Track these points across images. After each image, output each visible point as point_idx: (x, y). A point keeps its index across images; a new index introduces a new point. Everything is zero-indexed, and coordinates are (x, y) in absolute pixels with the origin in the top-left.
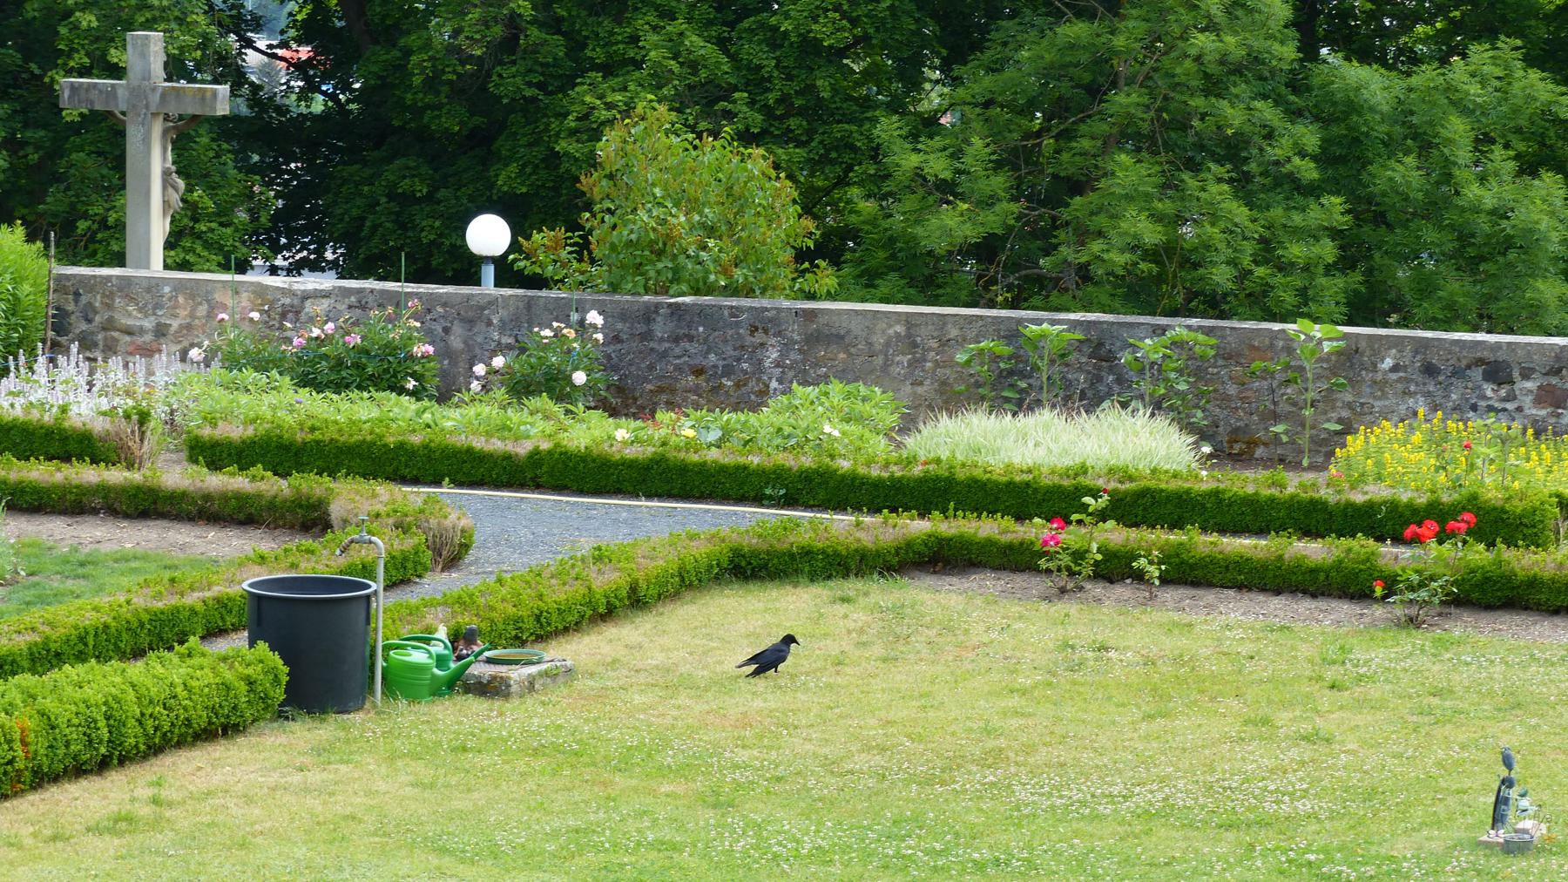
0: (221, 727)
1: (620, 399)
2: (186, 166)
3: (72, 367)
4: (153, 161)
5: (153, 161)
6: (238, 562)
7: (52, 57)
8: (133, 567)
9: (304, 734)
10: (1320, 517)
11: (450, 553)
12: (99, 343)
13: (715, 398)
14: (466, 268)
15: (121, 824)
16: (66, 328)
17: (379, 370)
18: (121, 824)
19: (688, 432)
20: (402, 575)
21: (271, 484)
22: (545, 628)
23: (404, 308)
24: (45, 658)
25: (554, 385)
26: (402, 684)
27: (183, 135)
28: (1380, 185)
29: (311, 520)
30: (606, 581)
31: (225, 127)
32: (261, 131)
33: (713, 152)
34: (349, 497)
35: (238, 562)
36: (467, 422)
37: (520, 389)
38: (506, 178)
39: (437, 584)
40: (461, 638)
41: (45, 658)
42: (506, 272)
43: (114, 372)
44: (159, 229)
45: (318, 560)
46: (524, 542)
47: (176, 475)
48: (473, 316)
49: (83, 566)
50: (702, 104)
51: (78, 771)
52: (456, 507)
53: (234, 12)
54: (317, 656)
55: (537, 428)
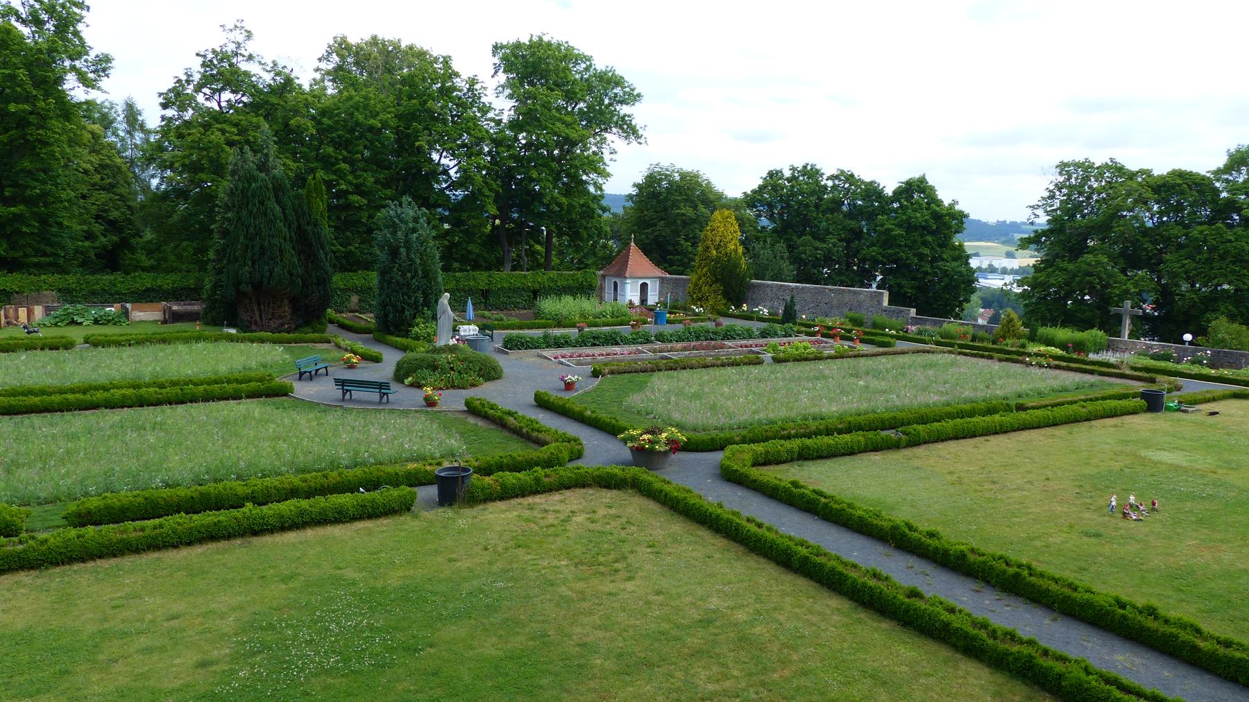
0: (1134, 412)
1: (1212, 366)
2: (1132, 322)
3: (1110, 353)
4: (1127, 322)
5: (1127, 322)
6: (1140, 387)
7: (1109, 304)
8: (1119, 385)
9: (1149, 415)
10: (1193, 196)
11: (1178, 389)
12: (1115, 350)
13: (1231, 366)
14: (1183, 342)
15: (1116, 426)
16: (1110, 347)
17: (1167, 358)
18: (1116, 426)
19: (1226, 372)
20: (1169, 391)
21: (1148, 374)
22: (1196, 402)
23: (1172, 348)
24: (1104, 398)
25: (1200, 363)
26: (1168, 409)
27: (1135, 319)
28: (890, 194)
29: (1153, 381)
30: (1209, 396)
31: (1139, 317)
32: (1146, 318)
33: (1235, 326)
34: (1159, 378)
35: (1140, 387)
36: (1183, 367)
37: (1193, 363)
38: (1191, 328)
39: (1175, 393)
40: (1180, 402)
41: (1104, 398)
42: (1191, 343)
43: (1118, 355)
44: (1127, 332)
45: (1154, 387)
46: (1192, 388)
47: (1128, 372)
48: (1185, 350)
49: (1111, 385)
50: (1232, 318)
51: (1109, 417)
52: (1180, 381)
53: (342, 201)
54: (1153, 403)
55: (1196, 369)
